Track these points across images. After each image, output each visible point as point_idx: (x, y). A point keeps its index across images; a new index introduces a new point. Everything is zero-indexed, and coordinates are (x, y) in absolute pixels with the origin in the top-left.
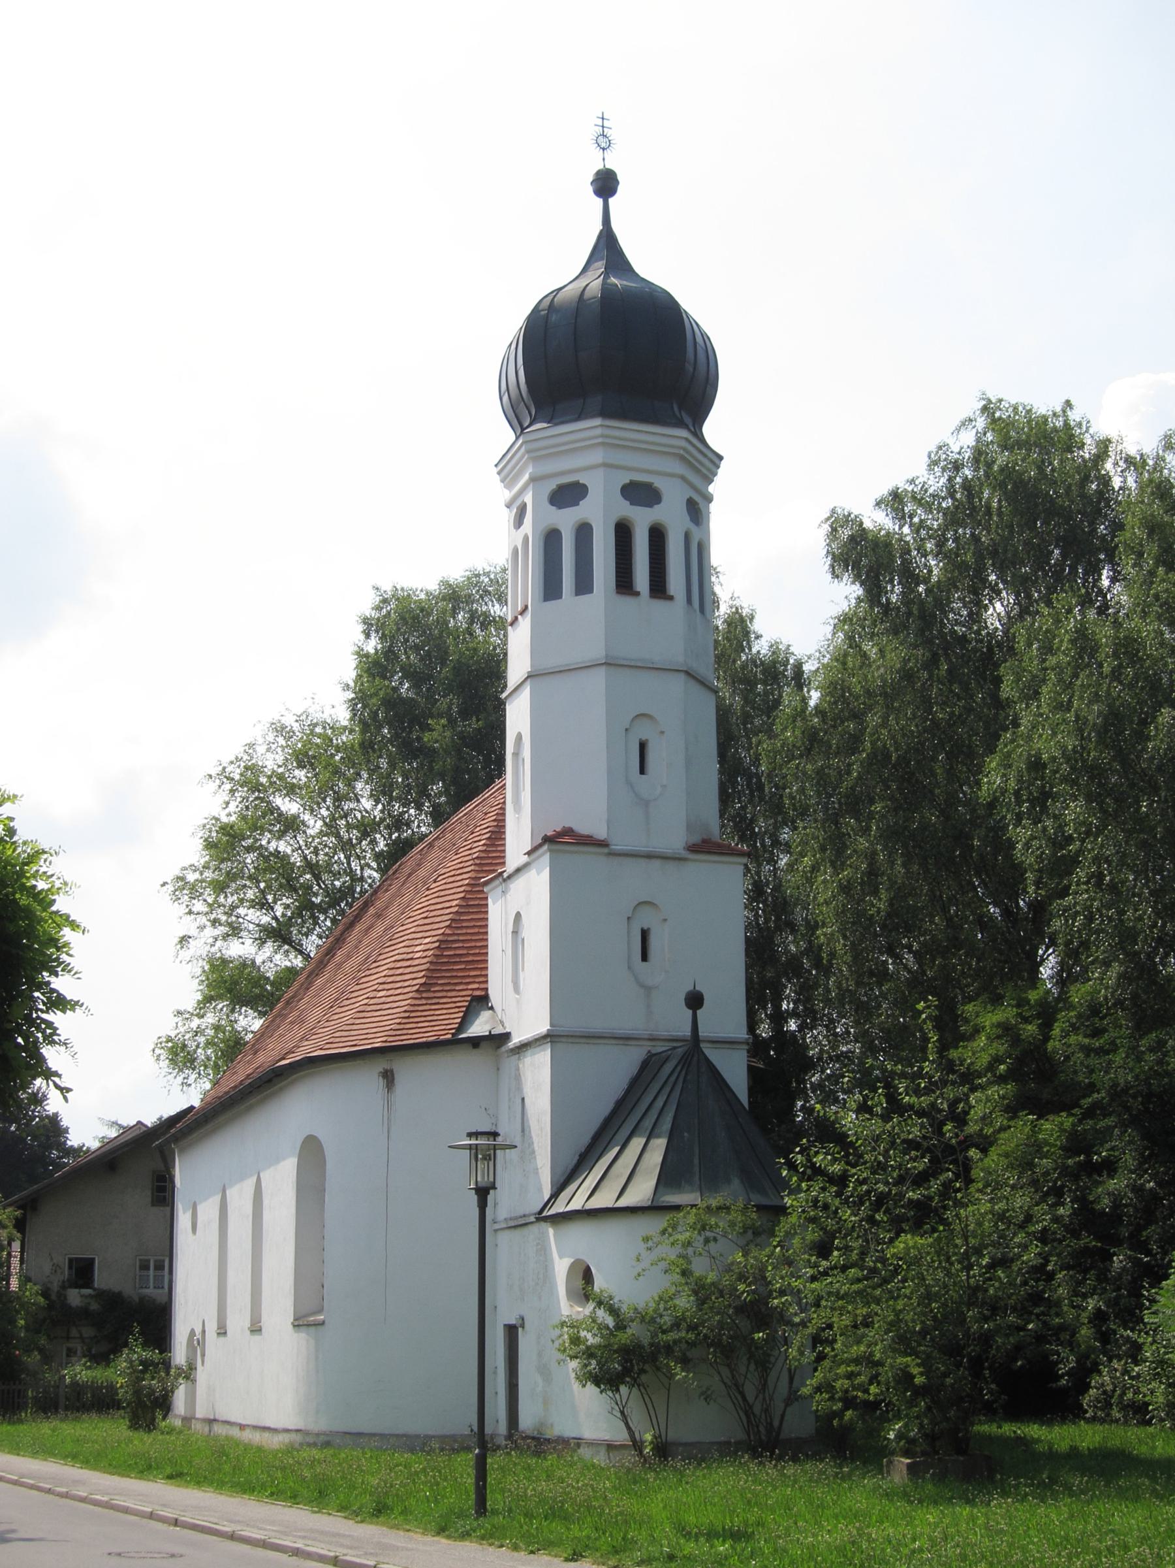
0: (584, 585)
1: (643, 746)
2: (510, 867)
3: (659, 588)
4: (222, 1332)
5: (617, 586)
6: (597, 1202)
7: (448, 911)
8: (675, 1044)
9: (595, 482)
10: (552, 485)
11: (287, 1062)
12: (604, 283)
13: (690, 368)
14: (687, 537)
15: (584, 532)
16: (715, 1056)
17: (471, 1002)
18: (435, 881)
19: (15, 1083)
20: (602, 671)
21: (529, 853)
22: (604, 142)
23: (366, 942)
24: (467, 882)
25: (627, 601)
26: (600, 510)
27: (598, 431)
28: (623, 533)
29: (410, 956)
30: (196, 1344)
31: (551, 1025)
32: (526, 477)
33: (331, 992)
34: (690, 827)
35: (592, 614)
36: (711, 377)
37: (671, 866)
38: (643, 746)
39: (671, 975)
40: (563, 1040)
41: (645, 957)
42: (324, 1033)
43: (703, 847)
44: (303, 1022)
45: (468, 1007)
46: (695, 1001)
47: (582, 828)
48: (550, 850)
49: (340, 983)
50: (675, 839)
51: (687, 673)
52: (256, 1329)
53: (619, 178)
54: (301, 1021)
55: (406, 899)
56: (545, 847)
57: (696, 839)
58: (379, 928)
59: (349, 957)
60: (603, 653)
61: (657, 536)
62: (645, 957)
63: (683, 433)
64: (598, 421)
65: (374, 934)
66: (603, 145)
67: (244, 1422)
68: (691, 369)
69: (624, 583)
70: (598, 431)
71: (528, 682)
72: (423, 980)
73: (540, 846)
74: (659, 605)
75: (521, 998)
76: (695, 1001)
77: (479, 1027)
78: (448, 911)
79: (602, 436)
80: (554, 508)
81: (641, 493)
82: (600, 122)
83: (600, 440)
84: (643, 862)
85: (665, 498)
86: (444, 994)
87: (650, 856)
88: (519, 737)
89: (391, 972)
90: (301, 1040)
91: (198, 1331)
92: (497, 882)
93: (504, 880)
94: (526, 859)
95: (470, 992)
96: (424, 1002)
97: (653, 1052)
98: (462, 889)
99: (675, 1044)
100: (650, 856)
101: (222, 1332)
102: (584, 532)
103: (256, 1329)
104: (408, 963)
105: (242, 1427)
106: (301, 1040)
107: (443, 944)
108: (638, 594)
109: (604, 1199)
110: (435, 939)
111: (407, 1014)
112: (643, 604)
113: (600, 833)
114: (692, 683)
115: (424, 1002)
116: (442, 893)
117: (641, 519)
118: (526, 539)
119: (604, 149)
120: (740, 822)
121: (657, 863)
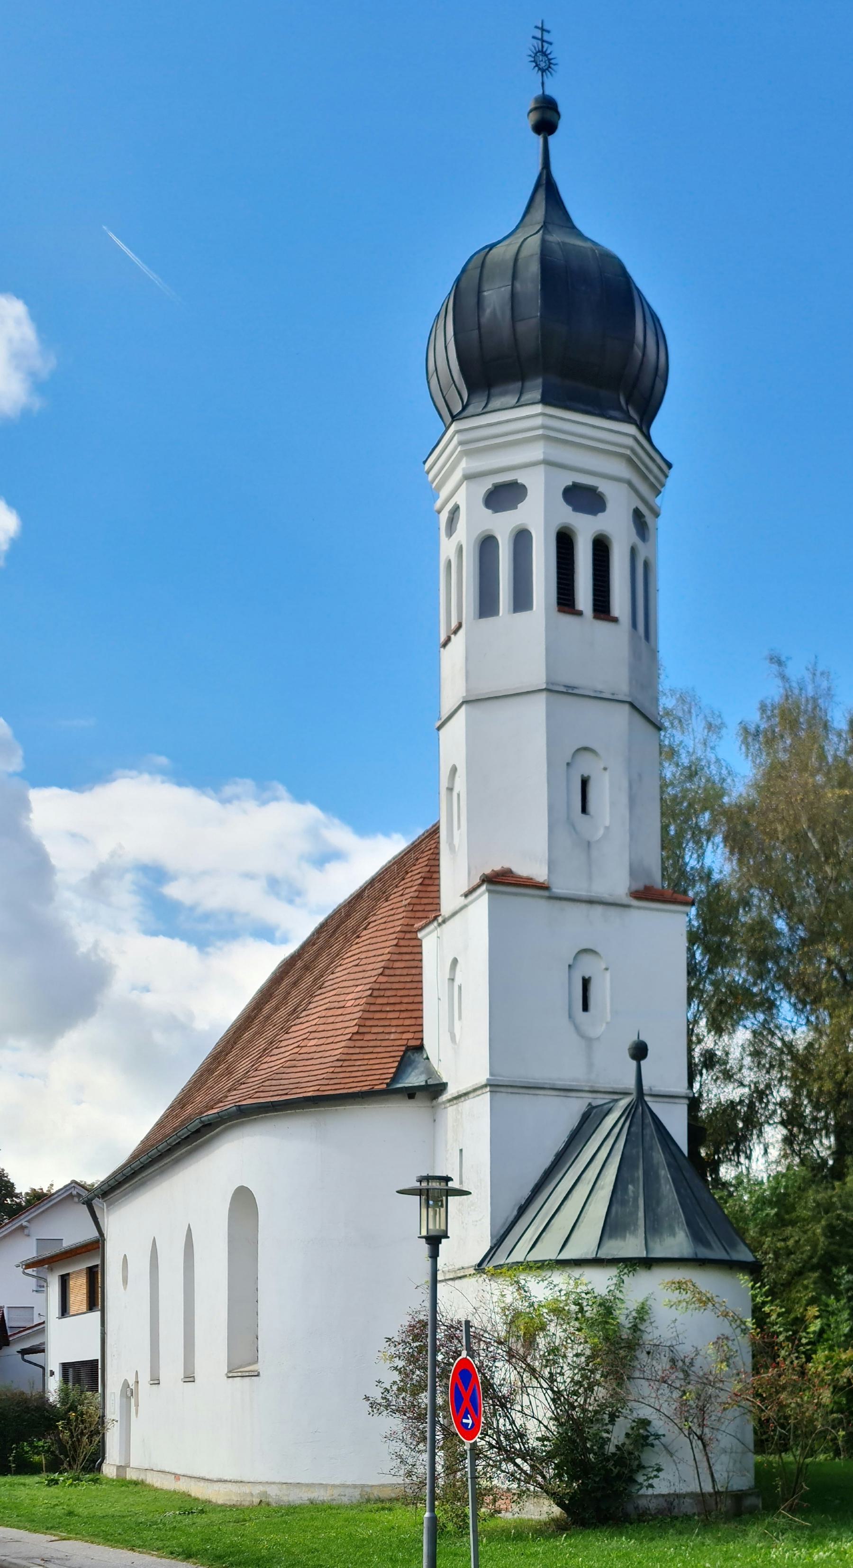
0: (522, 600)
1: (585, 783)
2: (446, 908)
3: (602, 607)
4: (156, 1381)
5: (559, 603)
6: (538, 1254)
7: (380, 958)
8: (616, 1097)
9: (536, 483)
10: (487, 484)
11: (215, 1111)
12: (543, 241)
13: (638, 352)
14: (633, 552)
15: (522, 538)
16: (657, 1108)
17: (405, 1052)
18: (365, 929)
19: (591, 1450)
20: (543, 696)
21: (466, 895)
22: (543, 61)
23: (294, 993)
24: (398, 929)
25: (567, 620)
26: (538, 515)
27: (539, 421)
28: (565, 542)
29: (341, 1004)
30: (129, 1393)
31: (491, 1074)
32: (458, 475)
33: (262, 1043)
34: (633, 873)
35: (527, 637)
36: (661, 371)
37: (613, 912)
38: (585, 783)
39: (613, 1021)
40: (502, 1089)
41: (585, 1008)
42: (254, 1081)
43: (646, 894)
44: (231, 1073)
45: (403, 1057)
46: (639, 1051)
47: (522, 870)
48: (489, 891)
49: (269, 1034)
50: (616, 882)
51: (632, 705)
52: (189, 1378)
53: (527, 498)
54: (229, 1072)
55: (335, 948)
56: (484, 888)
57: (639, 886)
58: (308, 979)
59: (277, 1009)
60: (544, 679)
61: (601, 549)
62: (585, 1008)
63: (632, 429)
64: (539, 408)
65: (303, 986)
66: (543, 65)
67: (178, 1472)
68: (640, 354)
69: (565, 599)
70: (539, 421)
71: (464, 708)
72: (355, 1029)
73: (478, 886)
74: (602, 626)
75: (458, 1042)
76: (639, 1051)
77: (414, 1079)
78: (380, 958)
79: (543, 427)
80: (490, 511)
81: (582, 497)
82: (538, 34)
83: (540, 432)
84: (584, 907)
85: (610, 506)
86: (378, 1043)
87: (591, 902)
88: (454, 770)
89: (322, 1020)
90: (229, 1091)
91: (131, 1382)
92: (432, 927)
93: (440, 925)
94: (463, 901)
95: (405, 1042)
96: (357, 1050)
97: (594, 1104)
98: (394, 936)
99: (616, 1097)
100: (591, 902)
101: (156, 1381)
102: (522, 538)
103: (189, 1378)
104: (340, 1011)
105: (177, 1477)
106: (229, 1091)
107: (375, 992)
108: (579, 613)
109: (548, 1251)
110: (368, 987)
111: (340, 1063)
112: (585, 627)
113: (540, 874)
114: (637, 718)
115: (357, 1050)
116: (374, 940)
117: (585, 528)
118: (460, 549)
119: (543, 71)
120: (679, 879)
121: (599, 910)
